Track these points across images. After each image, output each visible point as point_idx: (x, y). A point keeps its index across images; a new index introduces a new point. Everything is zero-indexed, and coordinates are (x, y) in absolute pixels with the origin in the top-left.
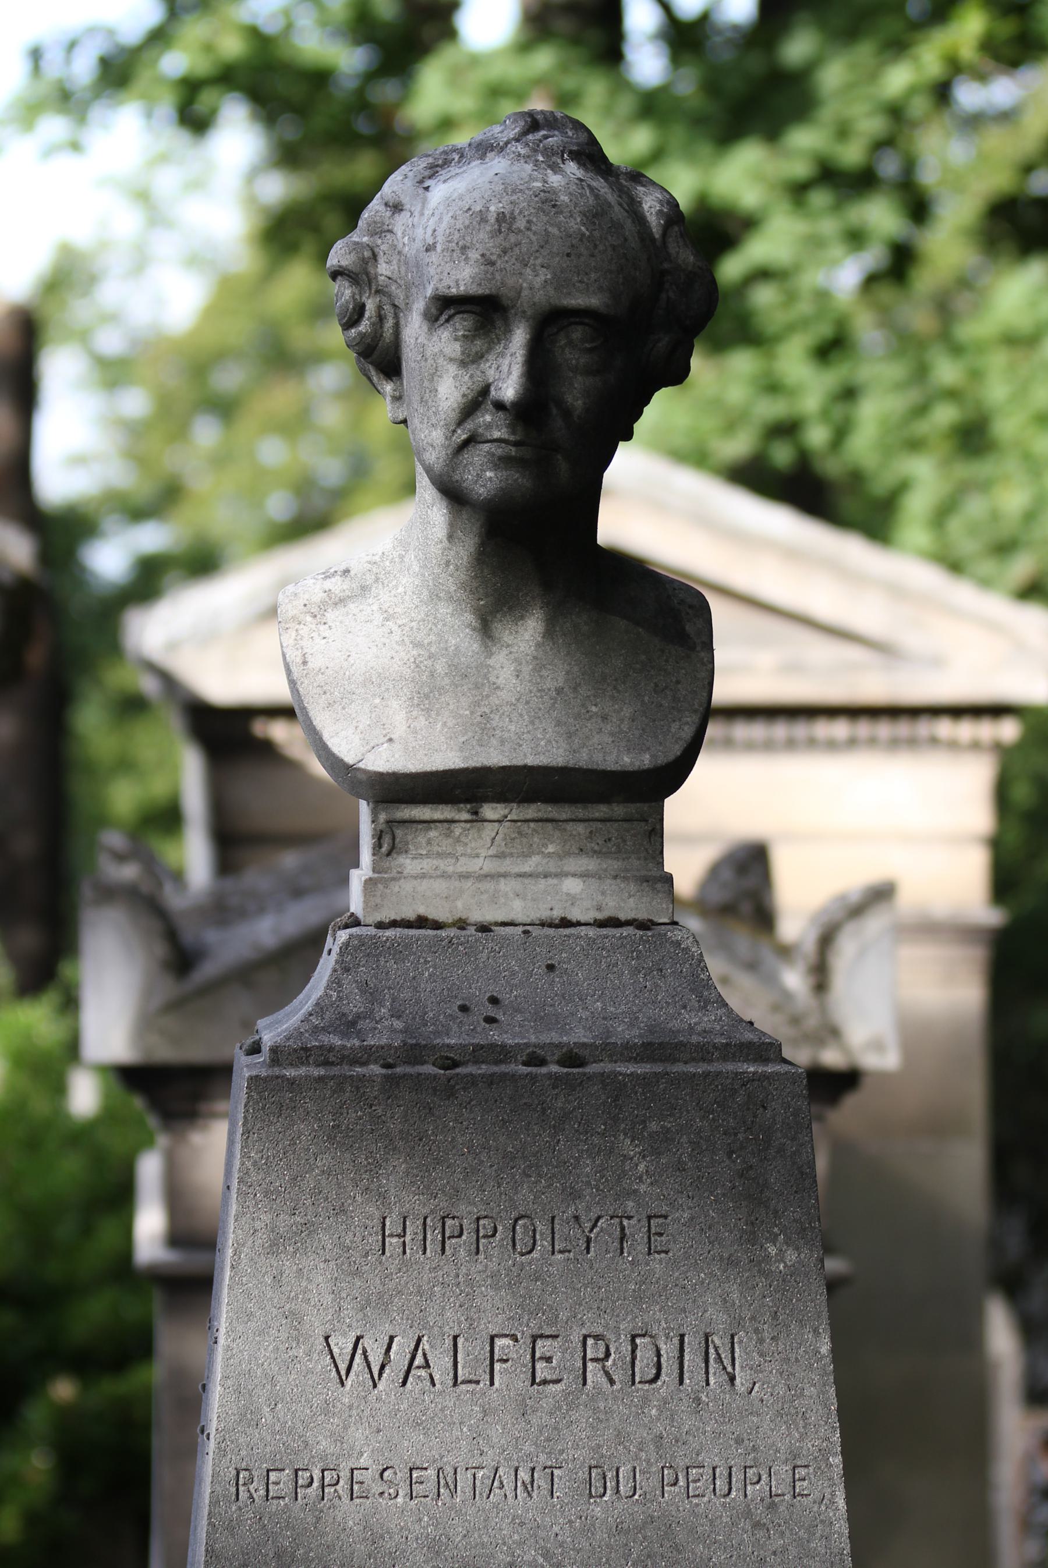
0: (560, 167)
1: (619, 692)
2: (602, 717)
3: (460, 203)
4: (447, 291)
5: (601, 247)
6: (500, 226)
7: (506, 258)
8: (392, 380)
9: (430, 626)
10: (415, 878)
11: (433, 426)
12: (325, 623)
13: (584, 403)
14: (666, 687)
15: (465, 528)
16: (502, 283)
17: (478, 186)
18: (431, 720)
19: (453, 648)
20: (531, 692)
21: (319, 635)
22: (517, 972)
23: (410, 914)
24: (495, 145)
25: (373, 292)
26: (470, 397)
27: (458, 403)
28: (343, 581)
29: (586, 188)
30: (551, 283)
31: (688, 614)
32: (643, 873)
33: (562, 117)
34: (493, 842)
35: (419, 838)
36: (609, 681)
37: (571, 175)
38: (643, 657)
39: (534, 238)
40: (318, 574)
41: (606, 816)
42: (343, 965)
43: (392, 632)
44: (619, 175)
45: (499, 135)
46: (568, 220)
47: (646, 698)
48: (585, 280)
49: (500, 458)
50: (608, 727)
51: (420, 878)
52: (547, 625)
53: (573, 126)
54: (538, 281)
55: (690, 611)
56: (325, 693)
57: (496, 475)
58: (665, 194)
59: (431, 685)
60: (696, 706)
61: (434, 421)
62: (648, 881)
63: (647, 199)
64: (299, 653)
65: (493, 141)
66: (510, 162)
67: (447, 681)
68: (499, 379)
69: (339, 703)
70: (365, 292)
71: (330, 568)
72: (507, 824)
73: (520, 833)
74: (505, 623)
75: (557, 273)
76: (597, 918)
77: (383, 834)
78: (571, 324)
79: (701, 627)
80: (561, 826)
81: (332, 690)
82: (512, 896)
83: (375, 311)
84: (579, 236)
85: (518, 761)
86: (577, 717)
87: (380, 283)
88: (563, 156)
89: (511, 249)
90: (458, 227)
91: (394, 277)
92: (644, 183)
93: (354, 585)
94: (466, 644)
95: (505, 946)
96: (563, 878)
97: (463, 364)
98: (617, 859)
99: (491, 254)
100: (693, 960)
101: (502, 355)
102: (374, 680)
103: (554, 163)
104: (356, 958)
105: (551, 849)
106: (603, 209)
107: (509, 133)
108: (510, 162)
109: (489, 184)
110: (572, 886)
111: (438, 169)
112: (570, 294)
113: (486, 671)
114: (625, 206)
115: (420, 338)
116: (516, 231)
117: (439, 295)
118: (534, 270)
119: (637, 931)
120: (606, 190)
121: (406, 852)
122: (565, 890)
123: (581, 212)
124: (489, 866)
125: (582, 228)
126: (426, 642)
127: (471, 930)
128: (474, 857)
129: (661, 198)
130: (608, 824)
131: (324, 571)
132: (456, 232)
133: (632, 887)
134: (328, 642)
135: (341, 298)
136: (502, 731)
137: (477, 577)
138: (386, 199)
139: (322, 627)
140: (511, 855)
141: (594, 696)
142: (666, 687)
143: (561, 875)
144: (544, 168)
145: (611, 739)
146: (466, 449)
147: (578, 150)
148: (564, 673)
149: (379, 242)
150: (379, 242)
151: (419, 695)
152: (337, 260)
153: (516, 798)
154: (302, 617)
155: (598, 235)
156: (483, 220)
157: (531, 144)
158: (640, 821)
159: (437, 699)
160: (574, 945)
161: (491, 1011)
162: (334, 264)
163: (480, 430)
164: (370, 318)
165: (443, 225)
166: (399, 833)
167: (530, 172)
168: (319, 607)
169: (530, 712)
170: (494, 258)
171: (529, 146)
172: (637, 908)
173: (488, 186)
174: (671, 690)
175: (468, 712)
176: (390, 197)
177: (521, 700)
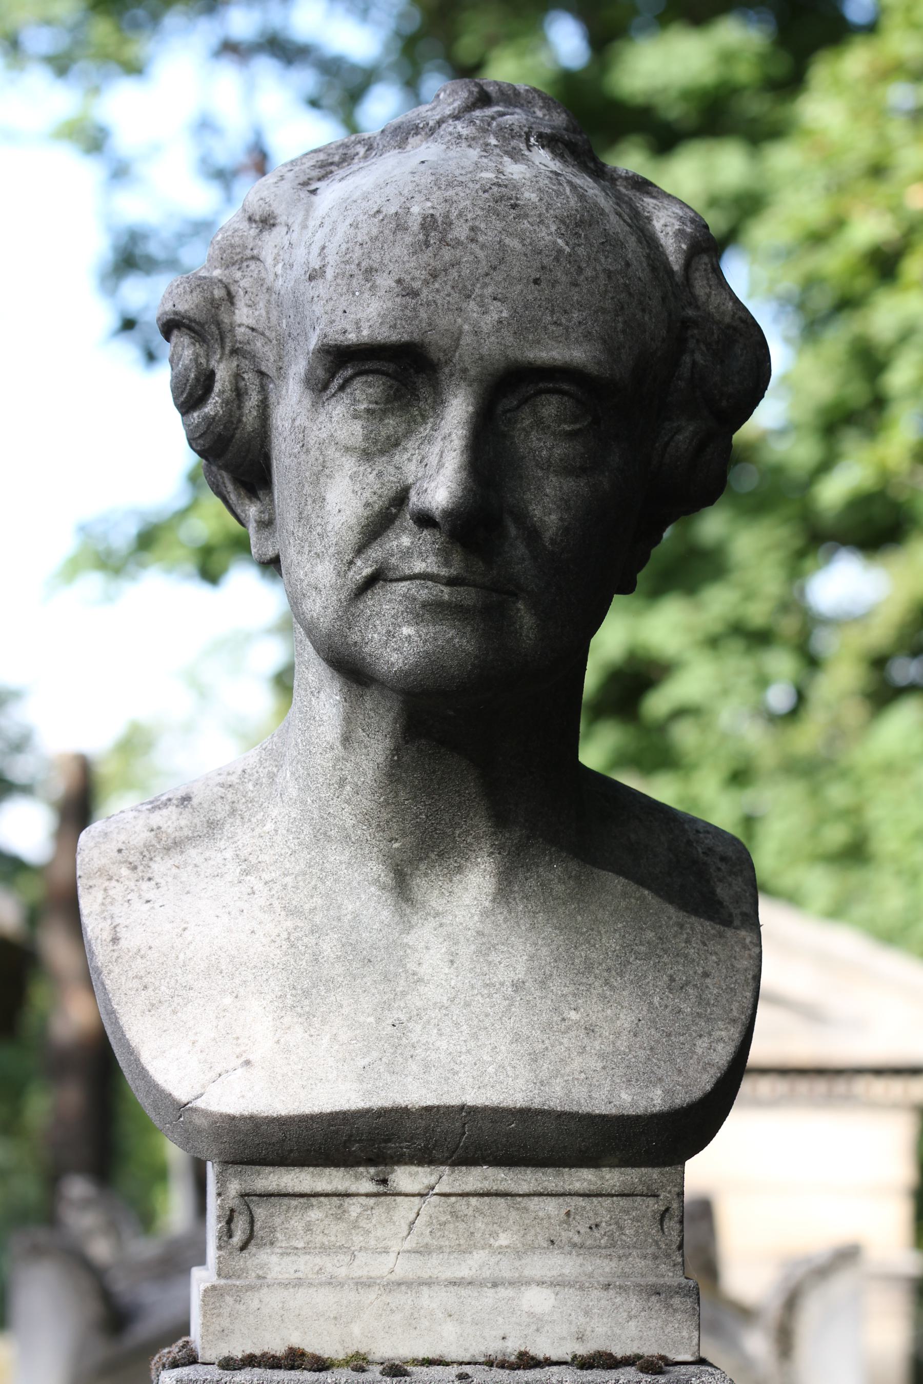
0: (523, 155)
1: (613, 988)
3: (364, 204)
4: (341, 338)
5: (589, 273)
6: (427, 236)
7: (437, 285)
8: (259, 499)
9: (313, 883)
10: (286, 1285)
11: (318, 556)
12: (150, 879)
13: (561, 519)
14: (687, 983)
15: (369, 725)
16: (430, 325)
17: (394, 180)
18: (312, 1031)
19: (349, 917)
20: (473, 987)
21: (140, 897)
23: (278, 1348)
24: (421, 125)
25: (227, 351)
26: (376, 507)
28: (181, 814)
29: (565, 185)
31: (719, 869)
32: (652, 1280)
33: (527, 91)
34: (411, 1229)
35: (292, 1222)
36: (597, 971)
37: (541, 166)
38: (650, 935)
39: (481, 254)
40: (142, 804)
41: (592, 1187)
43: (254, 893)
44: (616, 180)
45: (429, 113)
46: (535, 227)
47: (656, 1000)
48: (564, 321)
49: (424, 605)
50: (597, 1044)
51: (294, 1287)
52: (500, 882)
53: (544, 102)
55: (723, 866)
56: (146, 987)
57: (417, 632)
58: (687, 210)
59: (315, 975)
60: (735, 1013)
61: (319, 548)
62: (659, 1294)
63: (660, 214)
64: (107, 925)
65: (419, 121)
66: (444, 147)
67: (339, 969)
68: (424, 476)
69: (167, 1004)
70: (215, 352)
71: (162, 795)
73: (454, 1214)
74: (433, 877)
75: (518, 310)
76: (579, 1353)
77: (236, 1215)
78: (540, 392)
79: (739, 890)
80: (519, 1203)
81: (157, 983)
82: (441, 1315)
83: (230, 382)
84: (554, 253)
85: (452, 1099)
86: (548, 1027)
88: (528, 140)
89: (445, 270)
90: (359, 239)
91: (260, 327)
92: (654, 194)
94: (371, 910)
96: (523, 1288)
97: (367, 455)
99: (413, 279)
101: (429, 440)
102: (224, 967)
103: (514, 148)
105: (504, 1239)
106: (592, 215)
107: (444, 109)
108: (444, 147)
109: (411, 175)
111: (333, 168)
114: (626, 217)
115: (299, 419)
116: (453, 243)
117: (328, 345)
118: (482, 305)
119: (641, 1375)
120: (597, 192)
121: (272, 1244)
123: (556, 217)
124: (405, 1268)
126: (307, 907)
127: (375, 1372)
128: (380, 1253)
129: (681, 213)
130: (595, 1200)
131: (151, 799)
132: (357, 248)
133: (634, 1303)
134: (153, 908)
135: (178, 365)
137: (388, 804)
138: (250, 211)
139: (145, 885)
140: (440, 1249)
141: (574, 995)
142: (687, 983)
144: (498, 155)
145: (600, 1065)
146: (369, 591)
147: (552, 133)
148: (525, 958)
149: (238, 275)
151: (294, 992)
152: (171, 304)
153: (448, 1158)
154: (114, 869)
155: (585, 254)
156: (401, 227)
157: (478, 122)
158: (647, 1196)
159: (323, 998)
162: (167, 309)
163: (393, 560)
164: (222, 392)
165: (337, 238)
166: (260, 1213)
167: (476, 159)
168: (142, 853)
169: (471, 1019)
170: (416, 285)
171: (475, 124)
172: (641, 1338)
173: (410, 178)
174: (695, 986)
175: (371, 1019)
176: (256, 207)
177: (457, 1001)
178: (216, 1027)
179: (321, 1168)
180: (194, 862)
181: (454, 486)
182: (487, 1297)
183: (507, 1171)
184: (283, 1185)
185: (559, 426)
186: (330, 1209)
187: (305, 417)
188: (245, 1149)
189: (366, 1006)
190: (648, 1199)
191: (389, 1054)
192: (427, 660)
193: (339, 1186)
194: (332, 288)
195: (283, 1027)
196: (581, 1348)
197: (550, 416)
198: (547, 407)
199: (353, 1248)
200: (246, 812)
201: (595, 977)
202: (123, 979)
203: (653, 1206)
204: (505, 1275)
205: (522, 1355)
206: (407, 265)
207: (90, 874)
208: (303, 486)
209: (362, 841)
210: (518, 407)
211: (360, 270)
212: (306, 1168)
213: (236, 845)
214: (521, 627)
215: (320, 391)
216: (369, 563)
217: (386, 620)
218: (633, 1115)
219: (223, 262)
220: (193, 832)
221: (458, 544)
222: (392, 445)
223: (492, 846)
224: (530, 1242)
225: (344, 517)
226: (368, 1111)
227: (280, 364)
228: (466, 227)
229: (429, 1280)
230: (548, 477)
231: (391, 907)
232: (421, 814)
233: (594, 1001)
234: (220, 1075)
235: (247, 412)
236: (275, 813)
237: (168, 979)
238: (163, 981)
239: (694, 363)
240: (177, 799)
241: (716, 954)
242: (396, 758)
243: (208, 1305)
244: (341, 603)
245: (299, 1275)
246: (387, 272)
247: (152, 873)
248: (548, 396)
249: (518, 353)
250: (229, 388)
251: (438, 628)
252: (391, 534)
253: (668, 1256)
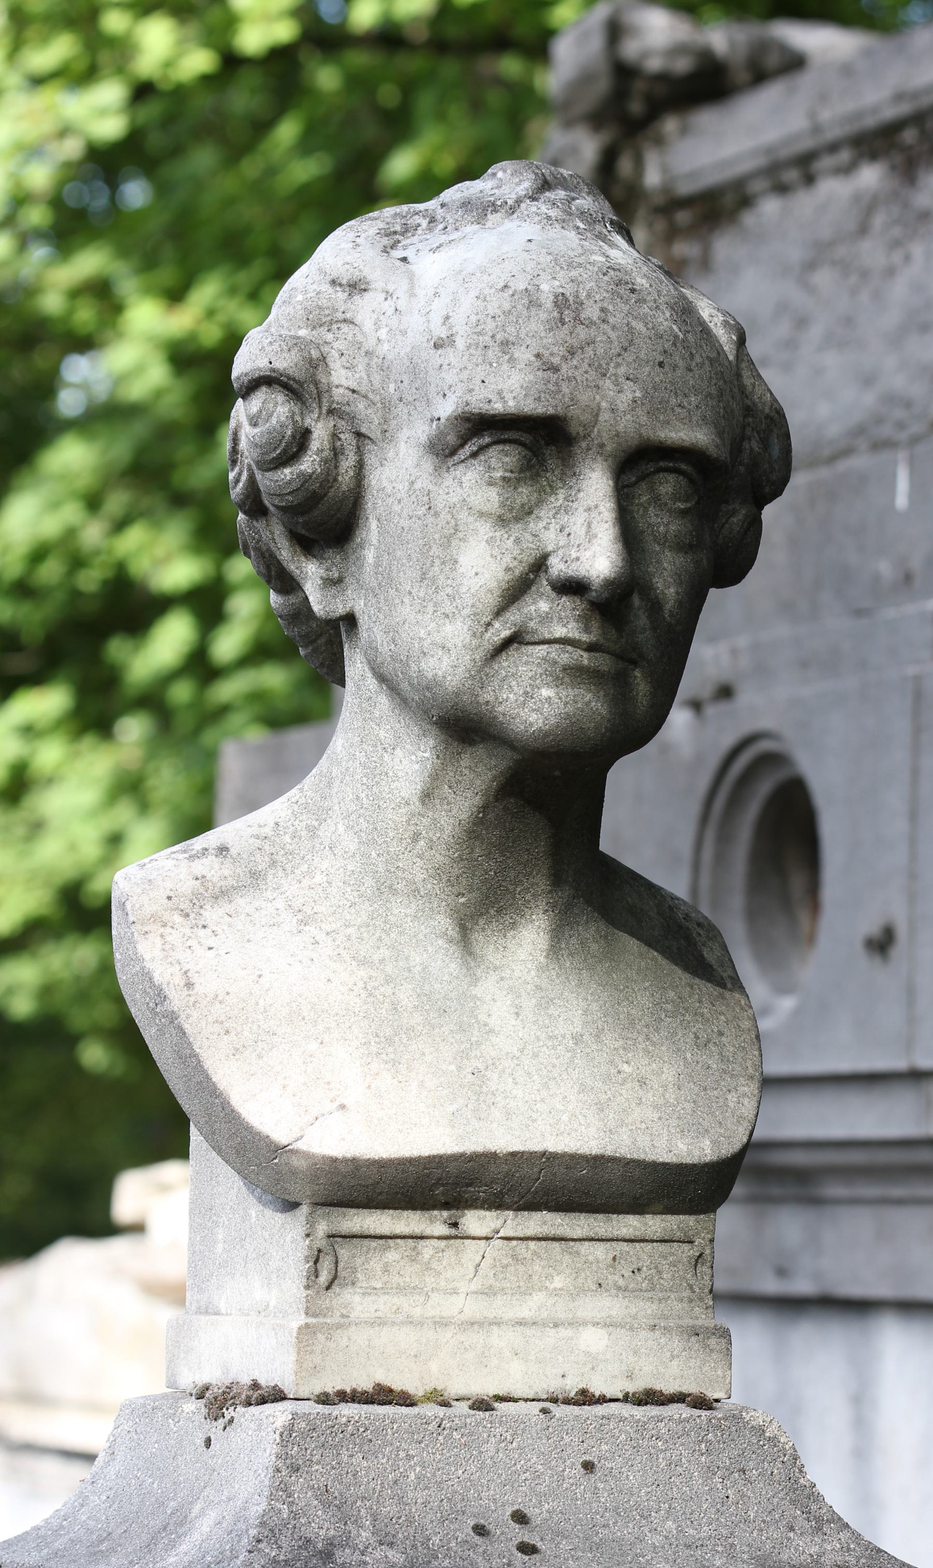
1: (654, 1044)
2: (638, 1081)
5: (698, 359)
7: (575, 362)
9: (377, 935)
13: (677, 593)
14: (709, 1041)
16: (572, 400)
18: (400, 1078)
19: (419, 968)
20: (538, 1039)
22: (542, 1473)
23: (366, 1385)
24: (499, 203)
25: (324, 411)
26: (517, 573)
27: (499, 582)
30: (643, 404)
31: (700, 935)
34: (477, 1271)
35: (372, 1263)
39: (613, 335)
41: (637, 1233)
42: (288, 1461)
46: (654, 312)
47: (689, 1055)
48: (686, 404)
49: (565, 669)
51: (379, 1325)
54: (624, 400)
57: (557, 694)
59: (396, 1023)
60: (751, 1071)
61: (448, 608)
62: (698, 1335)
69: (251, 1049)
72: (497, 1243)
74: (489, 933)
77: (322, 1255)
81: (239, 1029)
82: (509, 1354)
86: (607, 1079)
87: (336, 398)
89: (582, 348)
90: (491, 312)
91: (363, 389)
93: (239, 870)
94: (439, 962)
95: (520, 1432)
96: (581, 1329)
97: (502, 521)
100: (785, 1455)
102: (305, 1014)
104: (306, 1449)
105: (558, 1282)
112: (668, 423)
113: (472, 1004)
116: (587, 322)
121: (353, 1284)
124: (474, 1308)
125: (674, 327)
126: (376, 957)
127: (462, 1408)
128: (451, 1294)
132: (489, 320)
133: (676, 1343)
136: (506, 1098)
137: (462, 860)
139: (201, 933)
141: (624, 1049)
142: (709, 1041)
143: (575, 1323)
145: (656, 1116)
146: (504, 653)
148: (580, 1012)
149: (329, 337)
150: (329, 337)
151: (377, 1039)
152: (266, 361)
154: (166, 916)
156: (533, 303)
158: (684, 1242)
160: (616, 1431)
161: (521, 1534)
162: (261, 366)
163: (532, 624)
164: (320, 451)
166: (344, 1253)
170: (556, 360)
172: (682, 1376)
177: (526, 1052)
178: (305, 1072)
179: (400, 1211)
180: (246, 911)
181: (614, 556)
182: (549, 1337)
183: (563, 1217)
184: (366, 1226)
185: (674, 504)
186: (405, 1251)
187: (428, 481)
188: (338, 1191)
189: (447, 1055)
190: (684, 1245)
191: (473, 1101)
192: (568, 721)
193: (416, 1229)
194: (465, 358)
195: (372, 1073)
196: (631, 1386)
197: (667, 493)
198: (665, 485)
199: (426, 1289)
200: (287, 863)
201: (639, 1033)
202: (204, 1023)
203: (686, 1252)
204: (560, 1316)
205: (583, 1392)
206: (545, 341)
207: (144, 920)
208: (430, 547)
209: (431, 895)
210: (636, 483)
211: (495, 342)
212: (387, 1211)
213: (285, 896)
214: (637, 694)
215: (446, 457)
216: (508, 625)
217: (523, 681)
218: (690, 1164)
219: (309, 322)
220: (237, 882)
221: (597, 611)
222: (525, 513)
223: (547, 904)
224: (581, 1285)
225: (483, 580)
226: (462, 1155)
227: (385, 427)
228: (596, 308)
229: (494, 1320)
230: (664, 553)
231: (458, 960)
232: (491, 870)
233: (641, 1055)
234: (317, 1119)
235: (344, 471)
236: (325, 865)
237: (249, 1025)
238: (244, 1026)
239: (752, 450)
240: (214, 849)
241: (723, 1014)
242: (481, 815)
243: (302, 1342)
244: (476, 662)
245: (379, 1314)
246: (524, 346)
247: (205, 921)
248: (666, 474)
249: (651, 433)
250: (328, 447)
251: (576, 691)
252: (528, 598)
253: (701, 1299)
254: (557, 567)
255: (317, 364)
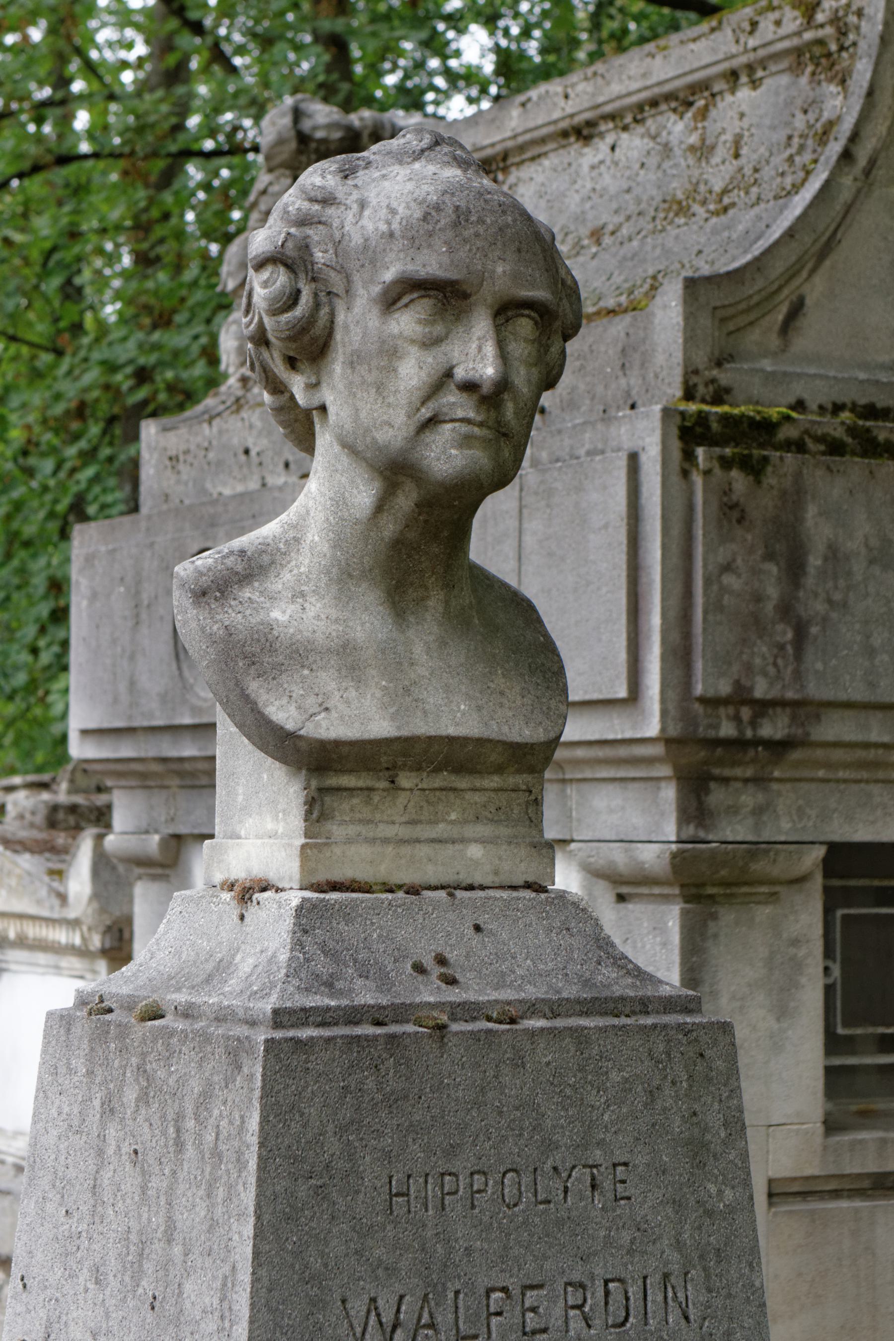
98: (507, 826)
110: (475, 851)
122: (469, 855)
124: (404, 832)
133: (523, 852)
143: (463, 841)
254: (460, 373)
255: (305, 247)
